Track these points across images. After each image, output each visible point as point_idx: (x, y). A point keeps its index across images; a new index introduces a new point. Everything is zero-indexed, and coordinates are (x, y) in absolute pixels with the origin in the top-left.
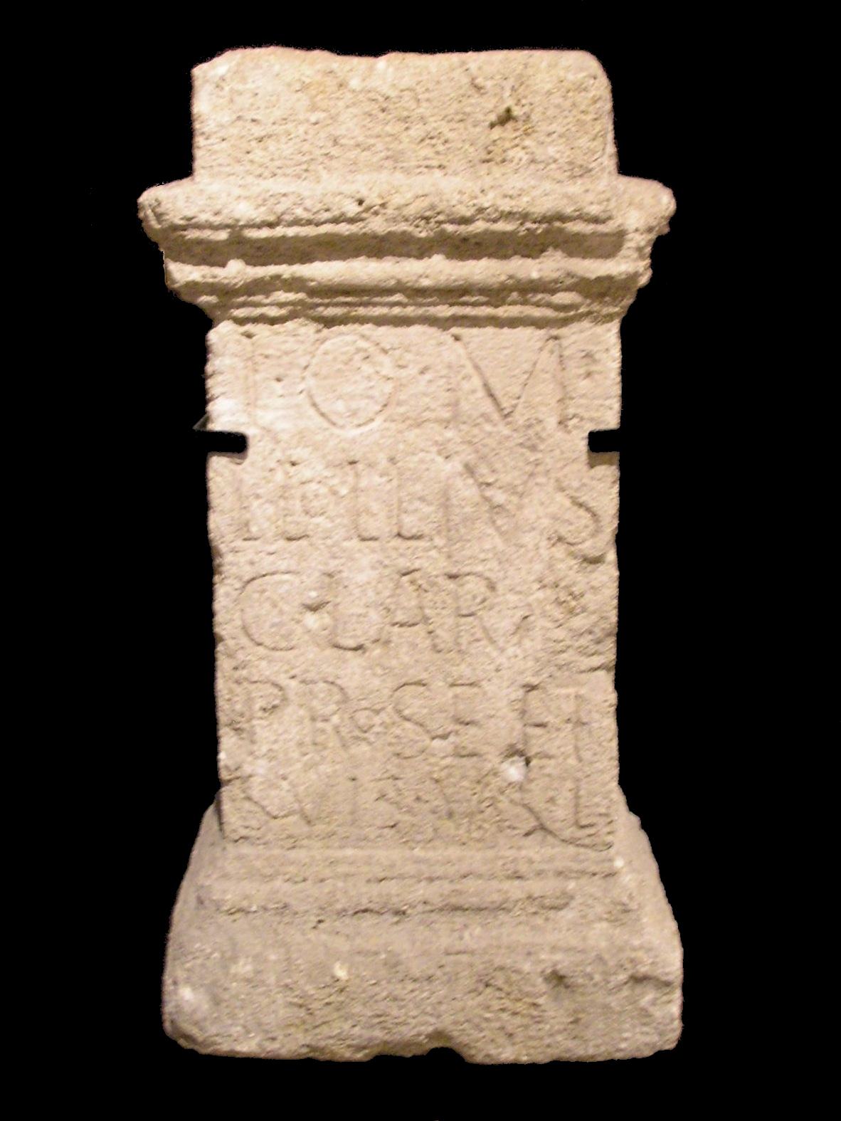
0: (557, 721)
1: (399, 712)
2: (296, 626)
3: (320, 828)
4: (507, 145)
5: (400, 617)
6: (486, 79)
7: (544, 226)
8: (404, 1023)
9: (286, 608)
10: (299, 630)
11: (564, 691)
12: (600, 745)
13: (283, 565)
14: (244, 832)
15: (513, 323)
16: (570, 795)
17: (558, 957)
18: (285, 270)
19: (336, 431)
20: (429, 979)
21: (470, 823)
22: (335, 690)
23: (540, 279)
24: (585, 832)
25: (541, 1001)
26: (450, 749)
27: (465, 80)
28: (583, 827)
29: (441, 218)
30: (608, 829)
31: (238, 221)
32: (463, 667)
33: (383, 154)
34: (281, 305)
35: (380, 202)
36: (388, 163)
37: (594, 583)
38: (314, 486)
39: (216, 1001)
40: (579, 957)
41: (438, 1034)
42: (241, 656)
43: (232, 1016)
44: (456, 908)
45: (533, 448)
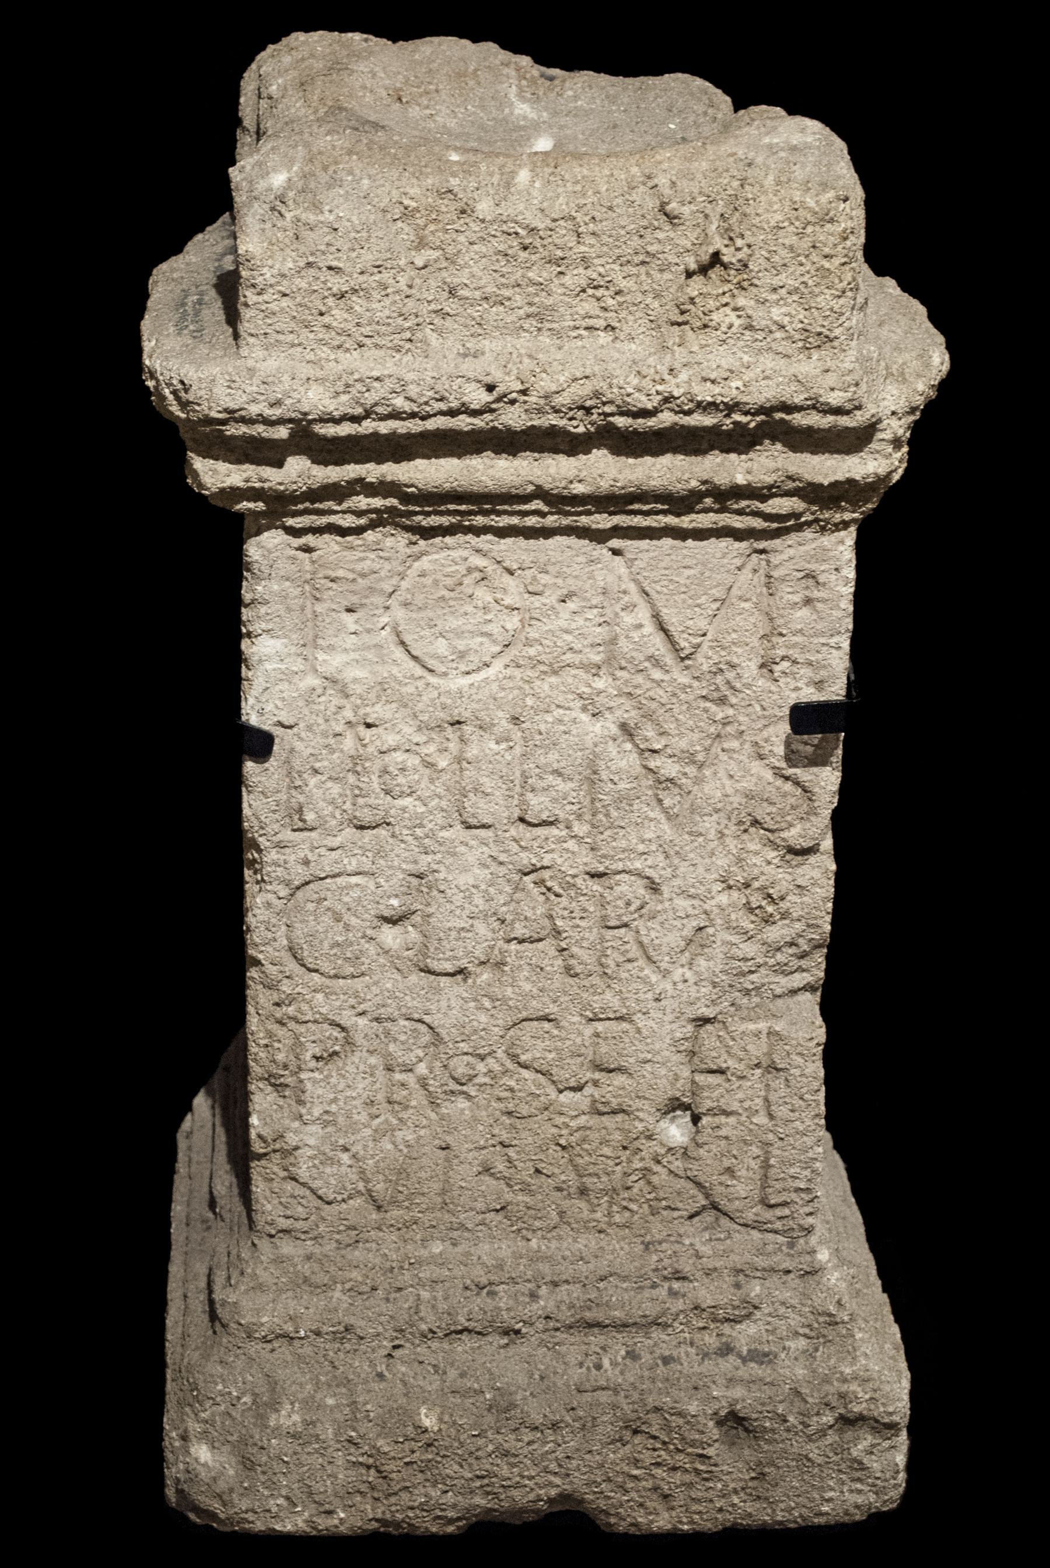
0: (742, 1067)
1: (514, 1057)
2: (367, 946)
3: (395, 1214)
4: (712, 304)
5: (520, 931)
6: (682, 203)
7: (760, 418)
8: (517, 1486)
9: (354, 921)
10: (372, 949)
11: (752, 1026)
12: (801, 1098)
13: (352, 865)
14: (283, 1223)
15: (700, 535)
16: (755, 1165)
17: (738, 1392)
18: (372, 471)
19: (433, 680)
20: (555, 1426)
21: (611, 1203)
22: (423, 1028)
23: (749, 485)
24: (778, 1212)
25: (710, 1452)
26: (585, 1105)
27: (651, 203)
28: (771, 1206)
29: (608, 409)
30: (808, 1209)
31: (306, 414)
32: (608, 995)
33: (521, 312)
34: (359, 514)
35: (520, 387)
36: (531, 324)
37: (800, 881)
38: (399, 756)
39: (248, 1464)
40: (769, 1391)
41: (564, 1497)
42: (286, 987)
43: (272, 1485)
44: (591, 1325)
45: (722, 701)
